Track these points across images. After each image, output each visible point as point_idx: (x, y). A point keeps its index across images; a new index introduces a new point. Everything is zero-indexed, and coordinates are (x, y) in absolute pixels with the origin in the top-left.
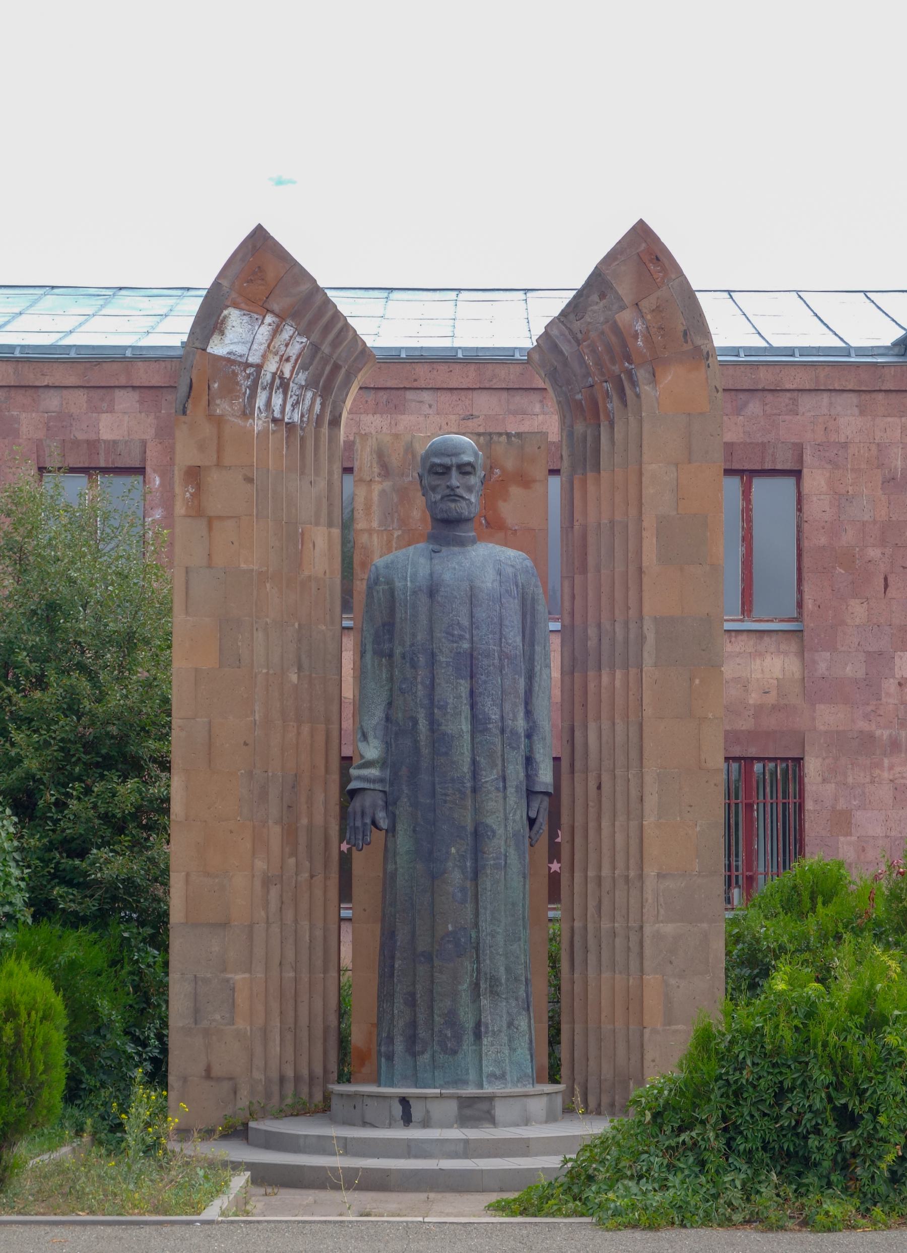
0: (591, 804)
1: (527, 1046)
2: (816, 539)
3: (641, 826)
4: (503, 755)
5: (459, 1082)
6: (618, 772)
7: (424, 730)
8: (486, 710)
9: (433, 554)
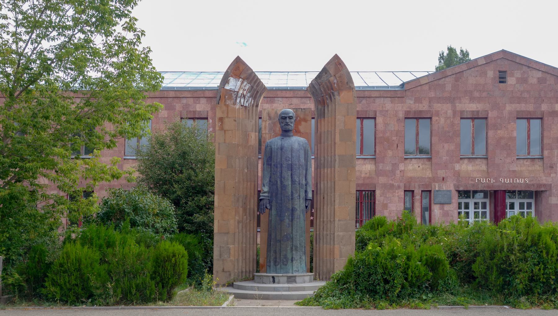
2: (379, 135)
5: (287, 272)
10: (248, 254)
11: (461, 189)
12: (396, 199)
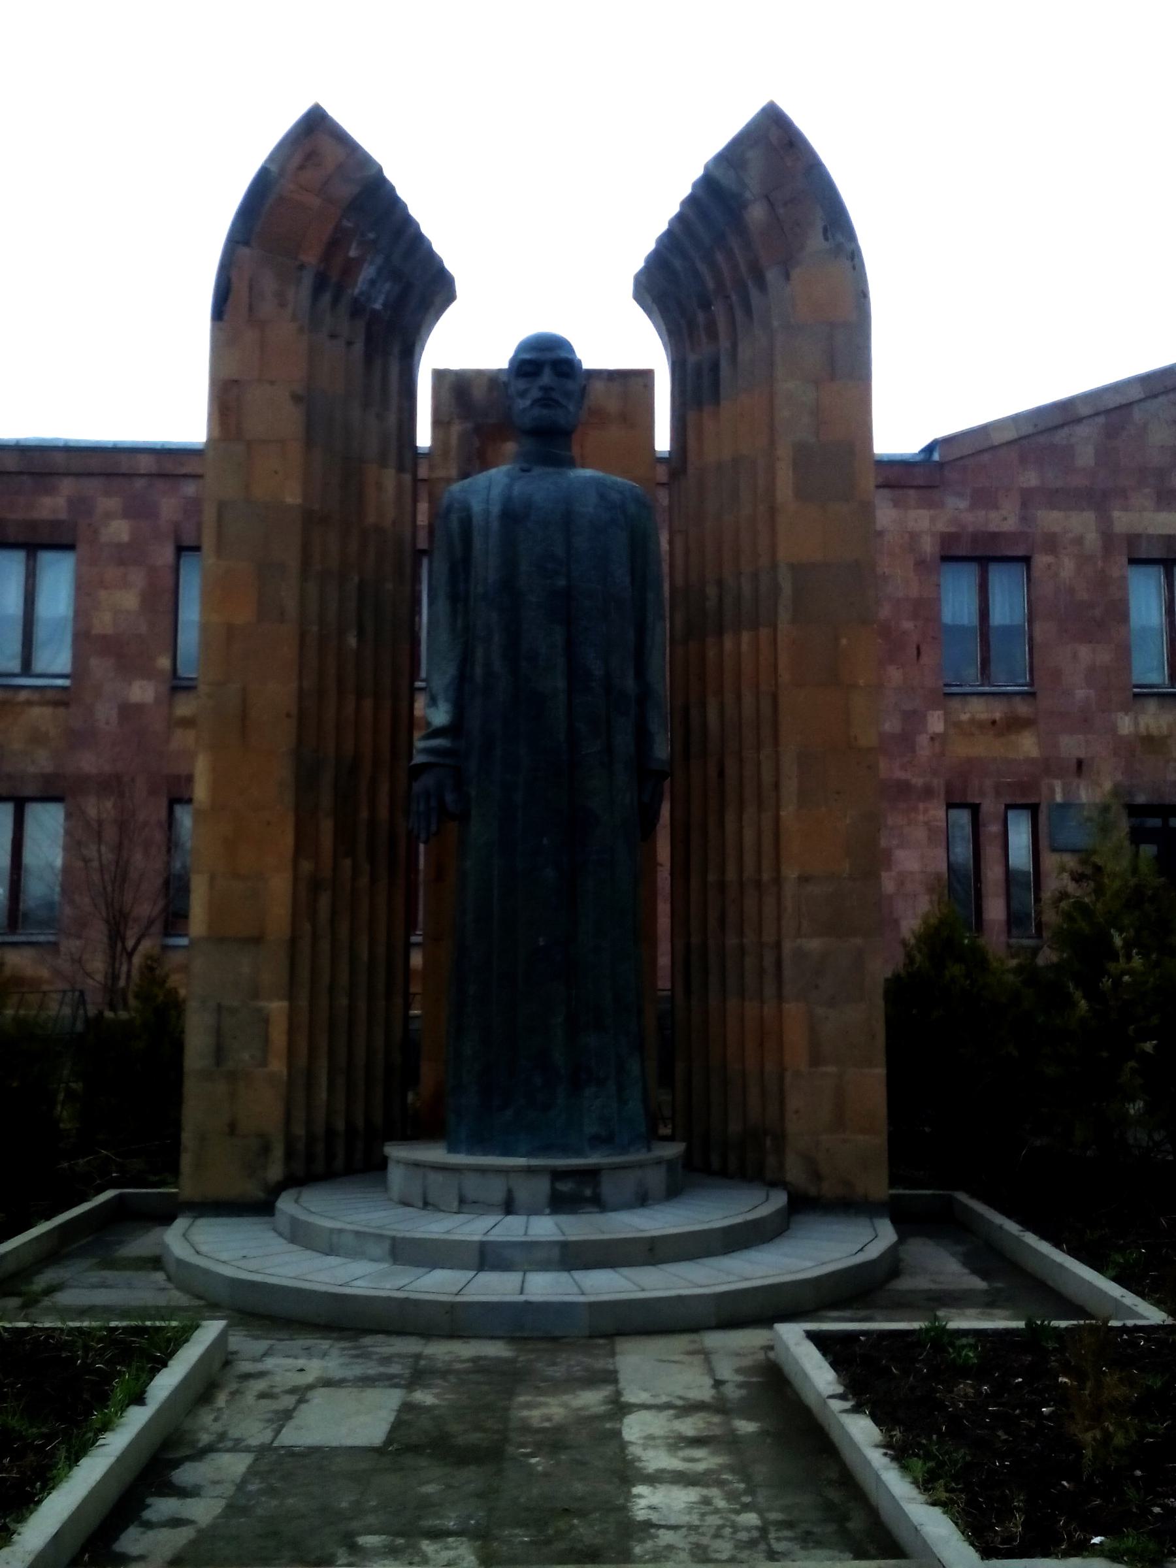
3: (777, 820)
11: (1141, 799)
12: (920, 834)
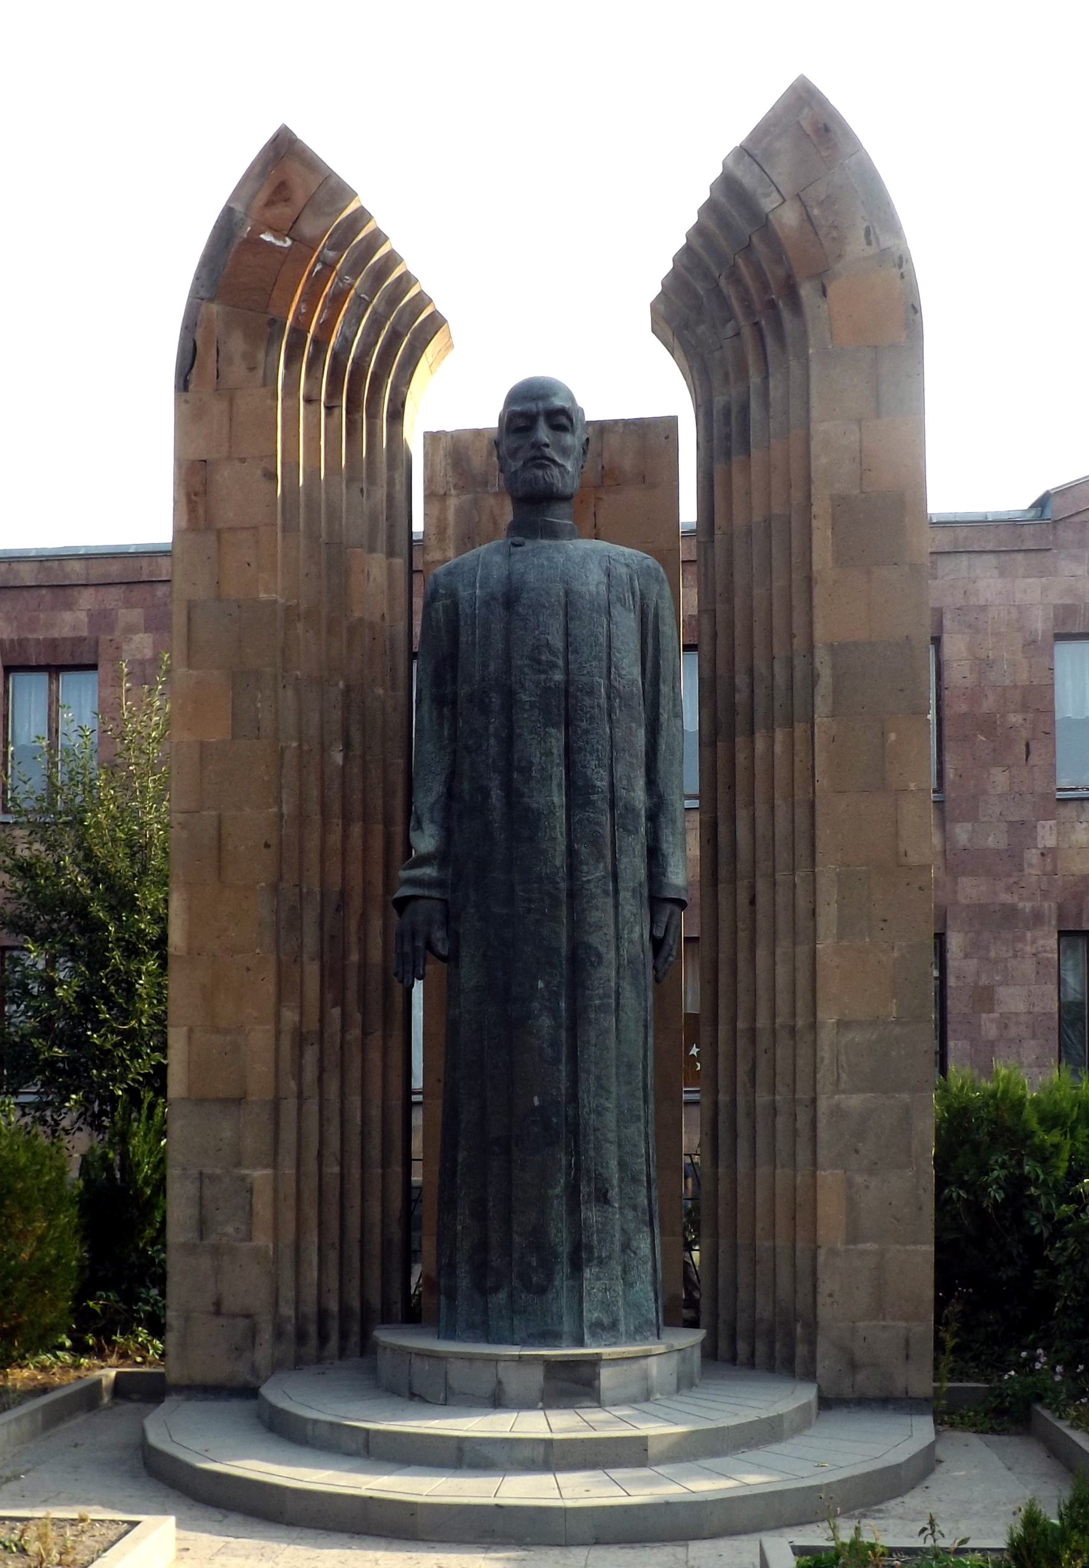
0: (740, 925)
1: (649, 1278)
2: (957, 707)
4: (613, 843)
5: (548, 1337)
6: (779, 876)
7: (498, 805)
8: (589, 773)
9: (513, 549)
10: (354, 1218)
12: (1028, 967)
